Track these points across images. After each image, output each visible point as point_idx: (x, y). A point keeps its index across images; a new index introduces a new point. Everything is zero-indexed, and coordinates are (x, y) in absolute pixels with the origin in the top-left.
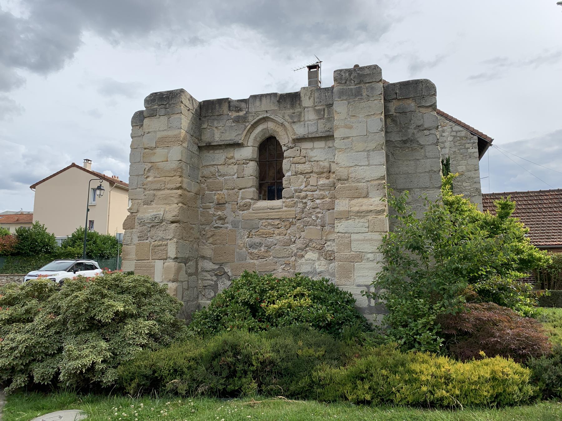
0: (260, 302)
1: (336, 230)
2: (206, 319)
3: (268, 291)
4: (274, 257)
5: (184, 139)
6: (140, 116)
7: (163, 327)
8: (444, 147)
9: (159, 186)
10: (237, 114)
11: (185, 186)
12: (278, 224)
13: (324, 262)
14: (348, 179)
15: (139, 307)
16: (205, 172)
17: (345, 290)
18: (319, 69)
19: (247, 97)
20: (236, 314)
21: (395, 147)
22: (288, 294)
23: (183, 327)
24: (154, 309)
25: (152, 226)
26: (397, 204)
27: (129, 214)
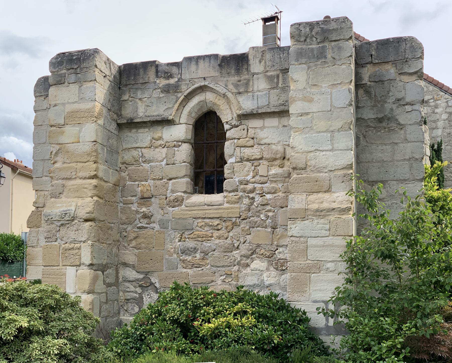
0: (193, 320)
1: (290, 234)
2: (127, 338)
3: (203, 306)
4: (212, 266)
5: (100, 114)
6: (45, 83)
7: (76, 346)
8: (437, 128)
9: (69, 173)
10: (167, 82)
11: (100, 174)
12: (218, 224)
13: (274, 273)
14: (305, 168)
15: (47, 323)
16: (126, 157)
17: (297, 307)
18: (279, 21)
19: (179, 59)
20: (163, 334)
21: (368, 126)
22: (227, 311)
23: (101, 348)
24: (65, 326)
25: (62, 225)
26: (368, 200)
27: (34, 209)
